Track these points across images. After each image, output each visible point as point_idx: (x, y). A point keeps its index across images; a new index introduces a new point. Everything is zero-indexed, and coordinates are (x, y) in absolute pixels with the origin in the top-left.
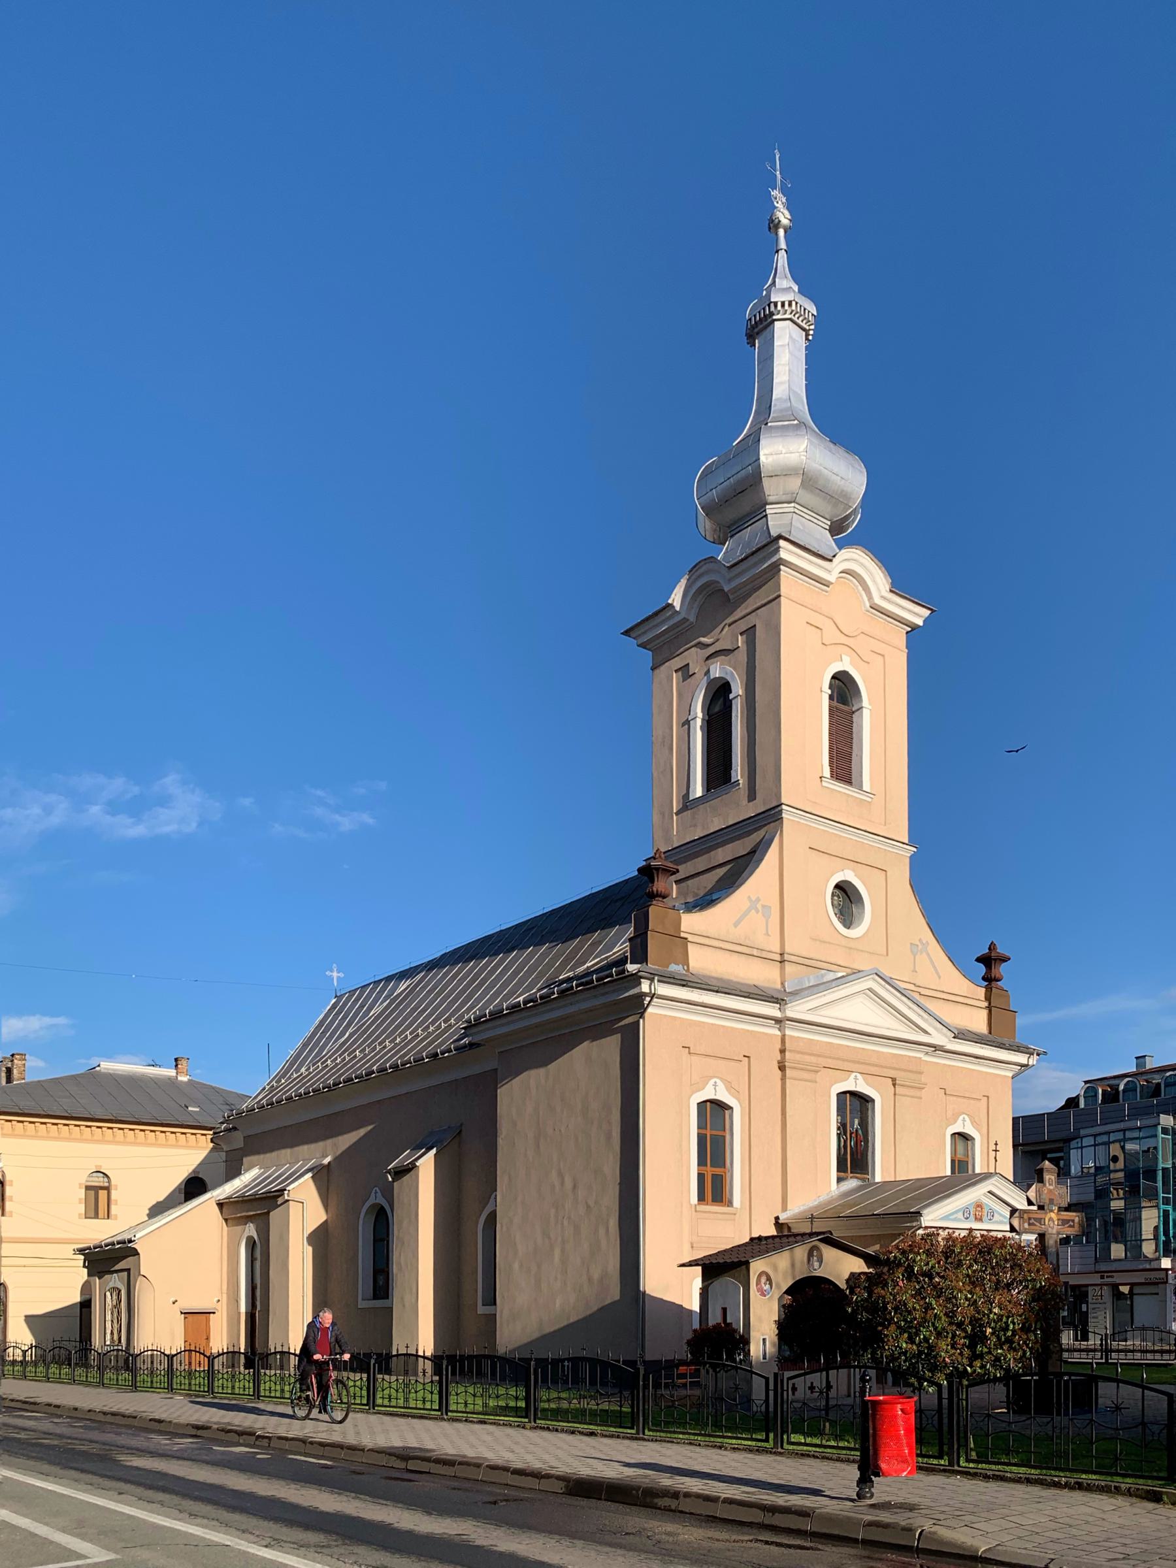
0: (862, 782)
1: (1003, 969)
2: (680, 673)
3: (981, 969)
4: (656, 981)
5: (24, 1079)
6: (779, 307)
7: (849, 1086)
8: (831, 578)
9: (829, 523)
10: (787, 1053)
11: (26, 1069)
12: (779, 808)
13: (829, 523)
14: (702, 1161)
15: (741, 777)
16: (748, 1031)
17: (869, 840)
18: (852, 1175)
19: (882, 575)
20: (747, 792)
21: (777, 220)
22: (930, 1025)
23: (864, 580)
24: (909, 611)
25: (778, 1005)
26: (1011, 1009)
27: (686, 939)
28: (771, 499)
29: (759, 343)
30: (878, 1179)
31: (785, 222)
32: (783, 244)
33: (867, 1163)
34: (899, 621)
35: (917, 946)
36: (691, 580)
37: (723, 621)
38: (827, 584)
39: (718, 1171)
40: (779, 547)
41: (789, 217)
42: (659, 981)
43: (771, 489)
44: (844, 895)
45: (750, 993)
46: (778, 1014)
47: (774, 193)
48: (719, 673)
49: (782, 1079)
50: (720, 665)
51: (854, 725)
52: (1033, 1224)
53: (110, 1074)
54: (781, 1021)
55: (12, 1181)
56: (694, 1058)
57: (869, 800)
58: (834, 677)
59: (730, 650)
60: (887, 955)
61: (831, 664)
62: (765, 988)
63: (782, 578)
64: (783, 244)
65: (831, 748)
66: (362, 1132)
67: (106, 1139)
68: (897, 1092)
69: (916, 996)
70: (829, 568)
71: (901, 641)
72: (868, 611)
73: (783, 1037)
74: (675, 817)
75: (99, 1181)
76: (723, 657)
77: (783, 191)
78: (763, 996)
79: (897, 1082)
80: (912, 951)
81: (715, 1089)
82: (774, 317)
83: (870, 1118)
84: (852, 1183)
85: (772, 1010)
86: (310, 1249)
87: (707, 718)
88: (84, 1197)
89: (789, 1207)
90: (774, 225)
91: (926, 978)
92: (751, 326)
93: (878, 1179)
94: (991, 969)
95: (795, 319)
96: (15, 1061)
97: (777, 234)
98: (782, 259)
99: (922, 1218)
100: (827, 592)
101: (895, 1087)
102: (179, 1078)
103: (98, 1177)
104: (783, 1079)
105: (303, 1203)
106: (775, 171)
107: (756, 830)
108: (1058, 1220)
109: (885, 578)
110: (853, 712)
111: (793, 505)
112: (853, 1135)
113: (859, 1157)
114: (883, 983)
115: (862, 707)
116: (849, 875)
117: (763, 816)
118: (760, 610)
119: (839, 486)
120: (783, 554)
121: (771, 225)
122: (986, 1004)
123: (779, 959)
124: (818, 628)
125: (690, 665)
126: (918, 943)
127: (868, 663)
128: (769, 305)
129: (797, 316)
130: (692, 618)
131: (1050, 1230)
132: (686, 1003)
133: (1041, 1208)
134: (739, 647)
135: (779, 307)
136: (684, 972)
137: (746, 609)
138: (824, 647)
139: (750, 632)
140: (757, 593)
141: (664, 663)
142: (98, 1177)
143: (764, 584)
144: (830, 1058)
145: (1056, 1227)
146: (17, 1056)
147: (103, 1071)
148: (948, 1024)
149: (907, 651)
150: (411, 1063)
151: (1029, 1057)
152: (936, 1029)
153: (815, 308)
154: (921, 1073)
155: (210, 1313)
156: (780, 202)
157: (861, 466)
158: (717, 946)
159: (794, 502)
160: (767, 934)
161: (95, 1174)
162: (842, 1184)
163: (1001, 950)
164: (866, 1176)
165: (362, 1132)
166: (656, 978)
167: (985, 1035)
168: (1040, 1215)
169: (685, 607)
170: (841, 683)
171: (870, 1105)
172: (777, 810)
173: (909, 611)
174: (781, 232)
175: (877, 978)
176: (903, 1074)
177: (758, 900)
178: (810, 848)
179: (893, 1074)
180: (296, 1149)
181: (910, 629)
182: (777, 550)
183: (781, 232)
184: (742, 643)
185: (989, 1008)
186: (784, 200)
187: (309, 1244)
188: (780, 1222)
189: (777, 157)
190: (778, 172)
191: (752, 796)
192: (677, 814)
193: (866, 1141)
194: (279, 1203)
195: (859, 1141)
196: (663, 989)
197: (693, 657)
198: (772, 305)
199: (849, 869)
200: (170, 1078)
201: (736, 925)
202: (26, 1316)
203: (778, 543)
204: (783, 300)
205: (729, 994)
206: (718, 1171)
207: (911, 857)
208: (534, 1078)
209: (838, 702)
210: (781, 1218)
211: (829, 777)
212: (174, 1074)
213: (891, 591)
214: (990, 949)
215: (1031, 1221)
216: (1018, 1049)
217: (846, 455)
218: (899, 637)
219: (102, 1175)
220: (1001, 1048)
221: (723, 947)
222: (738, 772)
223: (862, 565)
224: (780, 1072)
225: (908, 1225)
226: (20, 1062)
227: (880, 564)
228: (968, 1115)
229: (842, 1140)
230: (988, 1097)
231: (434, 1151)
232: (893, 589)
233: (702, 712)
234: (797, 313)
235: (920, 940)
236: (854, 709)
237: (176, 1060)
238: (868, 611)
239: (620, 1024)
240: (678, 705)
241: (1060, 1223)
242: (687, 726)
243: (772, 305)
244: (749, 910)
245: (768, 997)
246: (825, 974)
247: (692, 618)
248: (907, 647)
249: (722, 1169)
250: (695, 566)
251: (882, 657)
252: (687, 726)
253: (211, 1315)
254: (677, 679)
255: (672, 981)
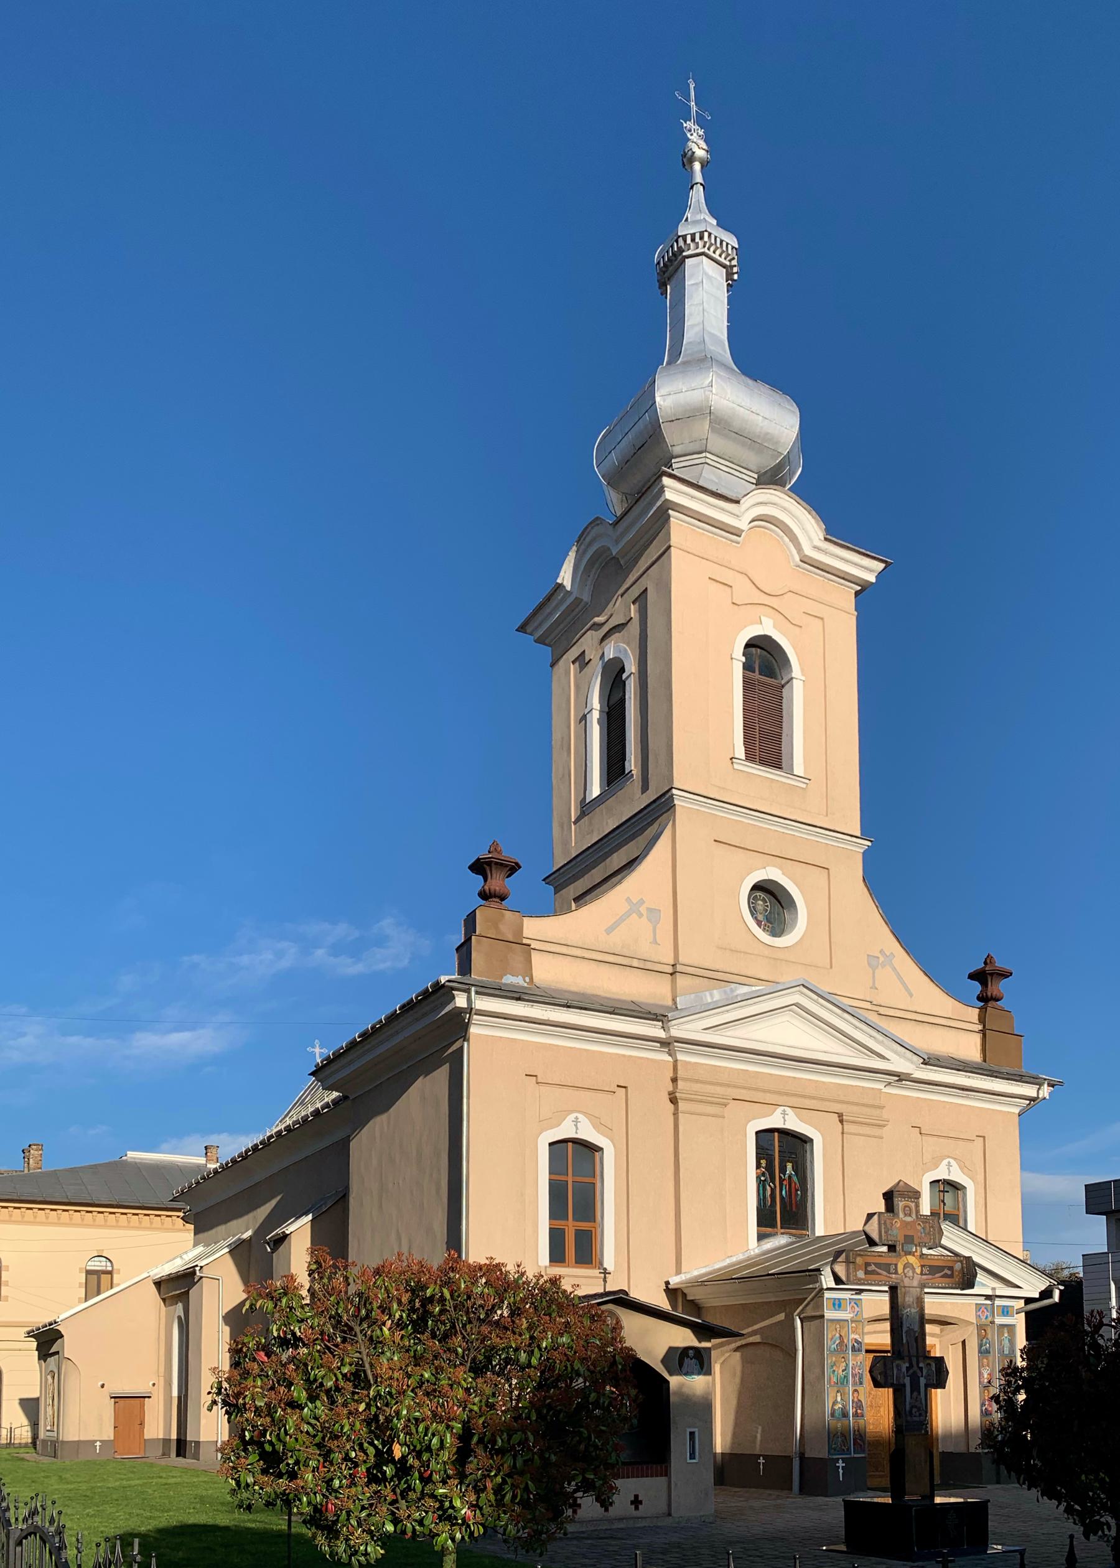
0: (792, 764)
1: (1002, 987)
2: (577, 664)
3: (977, 987)
4: (473, 993)
5: (41, 1168)
6: (689, 241)
7: (774, 1121)
8: (743, 524)
9: (756, 476)
10: (679, 1082)
11: (42, 1159)
12: (670, 794)
13: (756, 476)
14: (553, 1215)
15: (635, 767)
16: (624, 1056)
17: (803, 833)
18: (783, 1231)
19: (813, 521)
20: (641, 784)
21: (690, 152)
22: (888, 1048)
23: (788, 526)
24: (856, 564)
25: (660, 1023)
26: (1015, 1033)
27: (529, 945)
28: (677, 450)
29: (671, 289)
30: (820, 1231)
31: (700, 153)
32: (698, 178)
33: (806, 1216)
34: (843, 579)
35: (878, 958)
36: (581, 551)
37: (617, 592)
38: (737, 533)
39: (584, 1226)
40: (663, 487)
41: (705, 147)
42: (477, 993)
43: (674, 437)
44: (771, 897)
45: (615, 1008)
46: (662, 1034)
47: (688, 125)
48: (614, 653)
49: (674, 1114)
50: (614, 643)
51: (784, 701)
52: (873, 1272)
53: (136, 1163)
54: (669, 1044)
55: (8, 1266)
56: (543, 1088)
57: (804, 786)
58: (748, 645)
59: (623, 624)
60: (831, 967)
61: (745, 627)
62: (642, 1003)
63: (671, 523)
64: (698, 178)
65: (746, 727)
66: (274, 1202)
67: (108, 1224)
68: (845, 1130)
69: (873, 1018)
70: (738, 513)
71: (850, 603)
72: (799, 566)
73: (676, 1061)
74: (573, 827)
75: (99, 1265)
76: (617, 634)
77: (700, 121)
78: (641, 1012)
79: (844, 1117)
80: (869, 964)
81: (576, 1126)
82: (684, 254)
83: (808, 1161)
84: (780, 1240)
85: (654, 1030)
86: (227, 1329)
87: (607, 709)
88: (84, 1281)
89: (683, 1270)
90: (688, 159)
91: (891, 995)
92: (660, 269)
93: (820, 1231)
94: (986, 986)
95: (711, 253)
96: (32, 1151)
97: (691, 168)
98: (697, 195)
99: (822, 1277)
100: (738, 543)
101: (842, 1124)
102: (209, 1166)
103: (100, 1262)
104: (676, 1114)
105: (218, 1280)
106: (689, 101)
107: (650, 824)
108: (922, 1266)
109: (818, 524)
110: (783, 686)
111: (704, 455)
112: (784, 1183)
113: (794, 1209)
114: (815, 997)
115: (792, 678)
116: (773, 873)
117: (654, 805)
118: (651, 569)
119: (762, 427)
120: (669, 495)
121: (685, 160)
122: (980, 1027)
123: (671, 971)
124: (726, 585)
125: (586, 652)
126: (879, 955)
127: (801, 627)
128: (677, 241)
129: (712, 249)
130: (586, 597)
131: (907, 1282)
132: (526, 1022)
133: (892, 1248)
134: (631, 618)
135: (689, 241)
136: (526, 985)
137: (638, 572)
138: (736, 607)
139: (643, 596)
140: (648, 551)
141: (562, 656)
142: (100, 1262)
143: (654, 539)
144: (744, 1088)
145: (917, 1277)
146: (33, 1147)
147: (129, 1160)
148: (913, 1047)
149: (856, 613)
150: (299, 1123)
151: (1039, 1089)
152: (896, 1052)
153: (735, 240)
154: (882, 1108)
155: (145, 1397)
156: (695, 134)
157: (792, 406)
158: (580, 955)
159: (706, 451)
160: (655, 942)
161: (96, 1259)
162: (763, 1242)
163: (1000, 963)
164: (804, 1232)
165: (274, 1202)
166: (473, 989)
167: (976, 1063)
168: (891, 1259)
169: (576, 586)
170: (765, 653)
171: (808, 1146)
172: (667, 796)
173: (856, 564)
174: (697, 166)
175: (805, 990)
176: (855, 1109)
177: (642, 902)
178: (715, 841)
179: (838, 1108)
180: (229, 1224)
181: (860, 588)
182: (662, 490)
183: (697, 166)
184: (635, 611)
185: (983, 1032)
186: (701, 132)
187: (226, 1324)
188: (670, 1287)
189: (692, 86)
190: (693, 103)
191: (645, 788)
192: (575, 823)
193: (804, 1190)
194: (196, 1281)
195: (793, 1190)
196: (482, 1003)
197: (588, 642)
198: (681, 240)
199: (774, 866)
200: (198, 1166)
201: (609, 930)
202: (21, 1400)
203: (661, 481)
204: (692, 232)
205: (585, 1009)
206: (584, 1226)
207: (864, 853)
208: (378, 1125)
209: (760, 674)
210: (671, 1283)
211: (744, 758)
212: (204, 1162)
213: (826, 539)
214: (985, 963)
215: (869, 1269)
216: (1020, 1078)
217: (771, 392)
218: (846, 597)
219: (104, 1259)
220: (996, 1077)
221: (586, 956)
222: (632, 763)
223: (784, 509)
224: (672, 1105)
225: (811, 1286)
226: (36, 1152)
227: (809, 507)
228: (955, 1159)
229: (768, 1188)
230: (984, 1137)
231: (310, 1217)
232: (829, 537)
233: (600, 702)
234: (711, 245)
235: (881, 951)
236: (783, 682)
237: (206, 1148)
238: (799, 566)
239: (450, 1051)
240: (576, 700)
241: (925, 1270)
242: (584, 721)
243: (681, 240)
244: (628, 914)
245: (644, 1013)
246: (736, 989)
247: (586, 597)
248: (856, 610)
249: (563, 1222)
250: (583, 533)
251: (820, 620)
252: (584, 721)
253: (146, 1399)
254: (575, 669)
255: (497, 992)
